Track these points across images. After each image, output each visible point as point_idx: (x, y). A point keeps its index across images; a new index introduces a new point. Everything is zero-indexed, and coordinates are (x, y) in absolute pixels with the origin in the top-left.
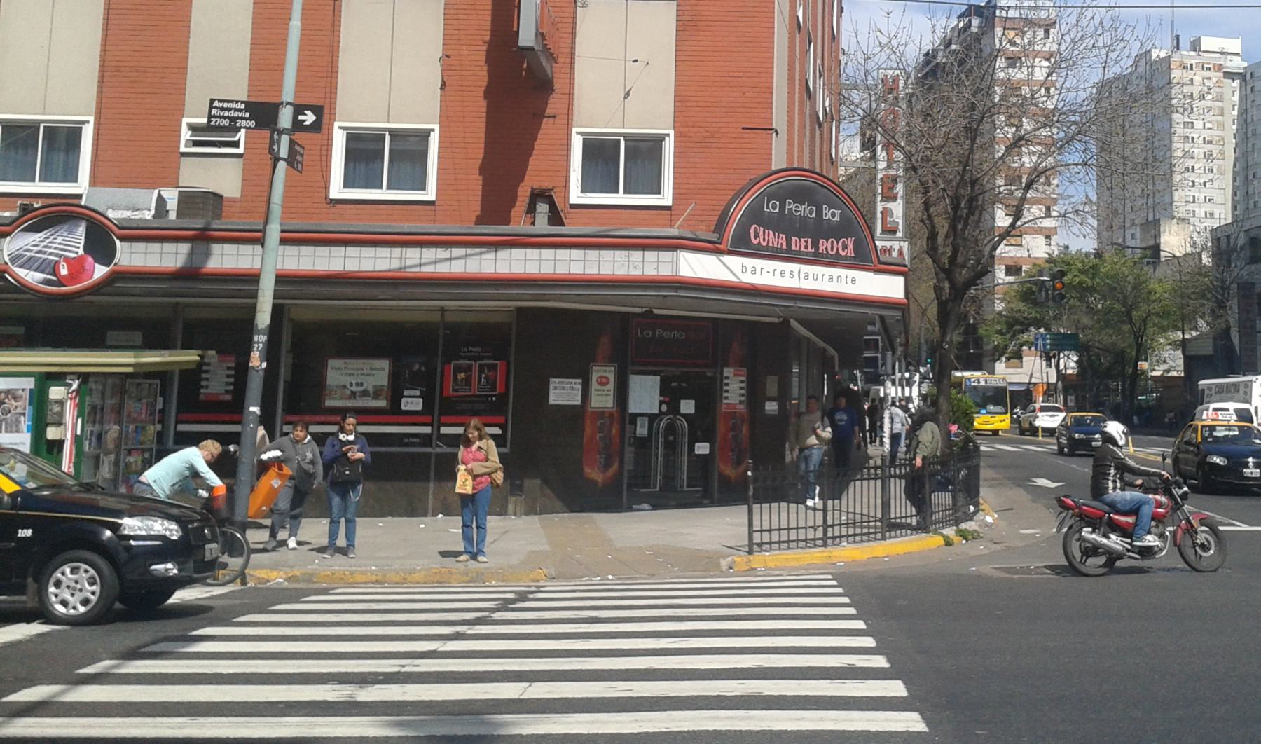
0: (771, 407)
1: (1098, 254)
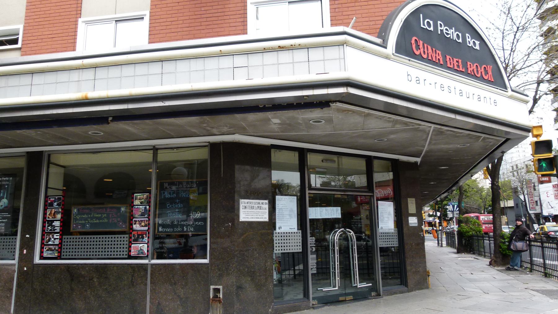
0: (413, 221)
1: (294, 187)
